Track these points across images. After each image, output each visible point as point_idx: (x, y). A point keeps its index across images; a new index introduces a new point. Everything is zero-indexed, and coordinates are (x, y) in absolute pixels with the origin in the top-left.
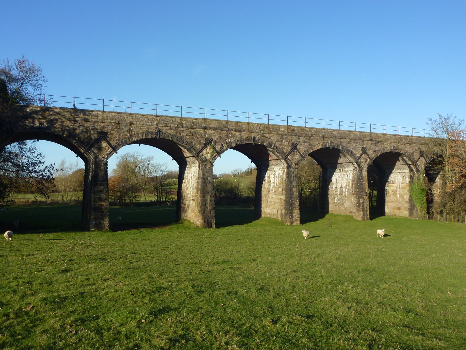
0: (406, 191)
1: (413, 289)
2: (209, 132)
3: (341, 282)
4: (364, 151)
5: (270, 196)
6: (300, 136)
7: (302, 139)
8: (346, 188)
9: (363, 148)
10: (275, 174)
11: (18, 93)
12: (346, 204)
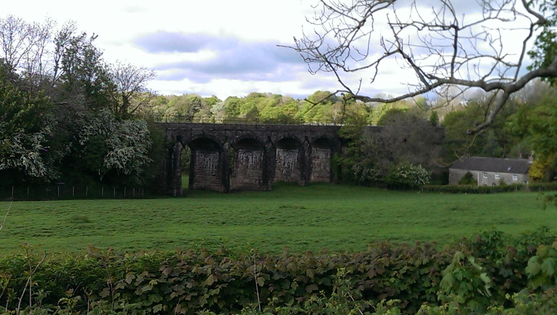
0: (328, 164)
1: (89, 53)
2: (228, 132)
3: (291, 240)
4: (306, 138)
5: (248, 170)
6: (272, 131)
7: (273, 133)
8: (292, 164)
9: (305, 137)
10: (253, 156)
11: (481, 240)
12: (293, 175)
